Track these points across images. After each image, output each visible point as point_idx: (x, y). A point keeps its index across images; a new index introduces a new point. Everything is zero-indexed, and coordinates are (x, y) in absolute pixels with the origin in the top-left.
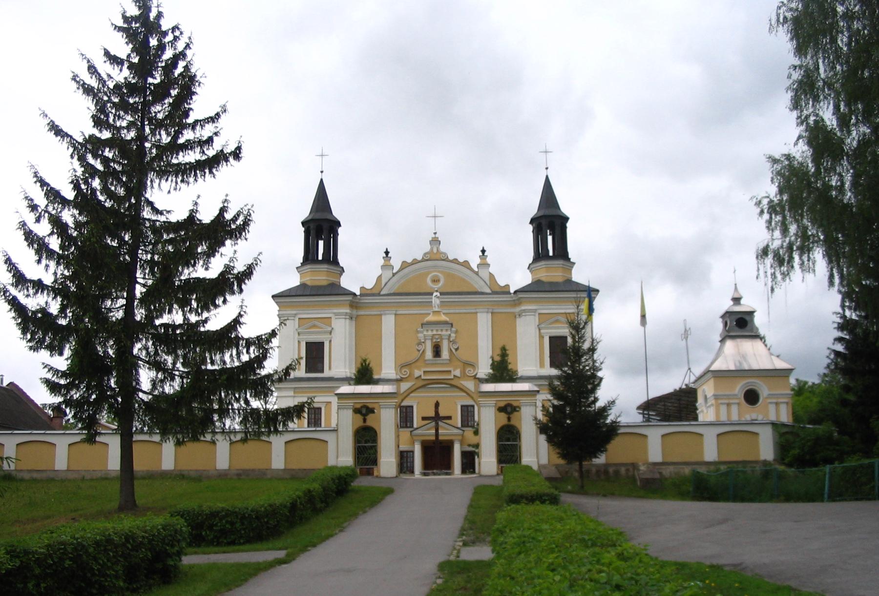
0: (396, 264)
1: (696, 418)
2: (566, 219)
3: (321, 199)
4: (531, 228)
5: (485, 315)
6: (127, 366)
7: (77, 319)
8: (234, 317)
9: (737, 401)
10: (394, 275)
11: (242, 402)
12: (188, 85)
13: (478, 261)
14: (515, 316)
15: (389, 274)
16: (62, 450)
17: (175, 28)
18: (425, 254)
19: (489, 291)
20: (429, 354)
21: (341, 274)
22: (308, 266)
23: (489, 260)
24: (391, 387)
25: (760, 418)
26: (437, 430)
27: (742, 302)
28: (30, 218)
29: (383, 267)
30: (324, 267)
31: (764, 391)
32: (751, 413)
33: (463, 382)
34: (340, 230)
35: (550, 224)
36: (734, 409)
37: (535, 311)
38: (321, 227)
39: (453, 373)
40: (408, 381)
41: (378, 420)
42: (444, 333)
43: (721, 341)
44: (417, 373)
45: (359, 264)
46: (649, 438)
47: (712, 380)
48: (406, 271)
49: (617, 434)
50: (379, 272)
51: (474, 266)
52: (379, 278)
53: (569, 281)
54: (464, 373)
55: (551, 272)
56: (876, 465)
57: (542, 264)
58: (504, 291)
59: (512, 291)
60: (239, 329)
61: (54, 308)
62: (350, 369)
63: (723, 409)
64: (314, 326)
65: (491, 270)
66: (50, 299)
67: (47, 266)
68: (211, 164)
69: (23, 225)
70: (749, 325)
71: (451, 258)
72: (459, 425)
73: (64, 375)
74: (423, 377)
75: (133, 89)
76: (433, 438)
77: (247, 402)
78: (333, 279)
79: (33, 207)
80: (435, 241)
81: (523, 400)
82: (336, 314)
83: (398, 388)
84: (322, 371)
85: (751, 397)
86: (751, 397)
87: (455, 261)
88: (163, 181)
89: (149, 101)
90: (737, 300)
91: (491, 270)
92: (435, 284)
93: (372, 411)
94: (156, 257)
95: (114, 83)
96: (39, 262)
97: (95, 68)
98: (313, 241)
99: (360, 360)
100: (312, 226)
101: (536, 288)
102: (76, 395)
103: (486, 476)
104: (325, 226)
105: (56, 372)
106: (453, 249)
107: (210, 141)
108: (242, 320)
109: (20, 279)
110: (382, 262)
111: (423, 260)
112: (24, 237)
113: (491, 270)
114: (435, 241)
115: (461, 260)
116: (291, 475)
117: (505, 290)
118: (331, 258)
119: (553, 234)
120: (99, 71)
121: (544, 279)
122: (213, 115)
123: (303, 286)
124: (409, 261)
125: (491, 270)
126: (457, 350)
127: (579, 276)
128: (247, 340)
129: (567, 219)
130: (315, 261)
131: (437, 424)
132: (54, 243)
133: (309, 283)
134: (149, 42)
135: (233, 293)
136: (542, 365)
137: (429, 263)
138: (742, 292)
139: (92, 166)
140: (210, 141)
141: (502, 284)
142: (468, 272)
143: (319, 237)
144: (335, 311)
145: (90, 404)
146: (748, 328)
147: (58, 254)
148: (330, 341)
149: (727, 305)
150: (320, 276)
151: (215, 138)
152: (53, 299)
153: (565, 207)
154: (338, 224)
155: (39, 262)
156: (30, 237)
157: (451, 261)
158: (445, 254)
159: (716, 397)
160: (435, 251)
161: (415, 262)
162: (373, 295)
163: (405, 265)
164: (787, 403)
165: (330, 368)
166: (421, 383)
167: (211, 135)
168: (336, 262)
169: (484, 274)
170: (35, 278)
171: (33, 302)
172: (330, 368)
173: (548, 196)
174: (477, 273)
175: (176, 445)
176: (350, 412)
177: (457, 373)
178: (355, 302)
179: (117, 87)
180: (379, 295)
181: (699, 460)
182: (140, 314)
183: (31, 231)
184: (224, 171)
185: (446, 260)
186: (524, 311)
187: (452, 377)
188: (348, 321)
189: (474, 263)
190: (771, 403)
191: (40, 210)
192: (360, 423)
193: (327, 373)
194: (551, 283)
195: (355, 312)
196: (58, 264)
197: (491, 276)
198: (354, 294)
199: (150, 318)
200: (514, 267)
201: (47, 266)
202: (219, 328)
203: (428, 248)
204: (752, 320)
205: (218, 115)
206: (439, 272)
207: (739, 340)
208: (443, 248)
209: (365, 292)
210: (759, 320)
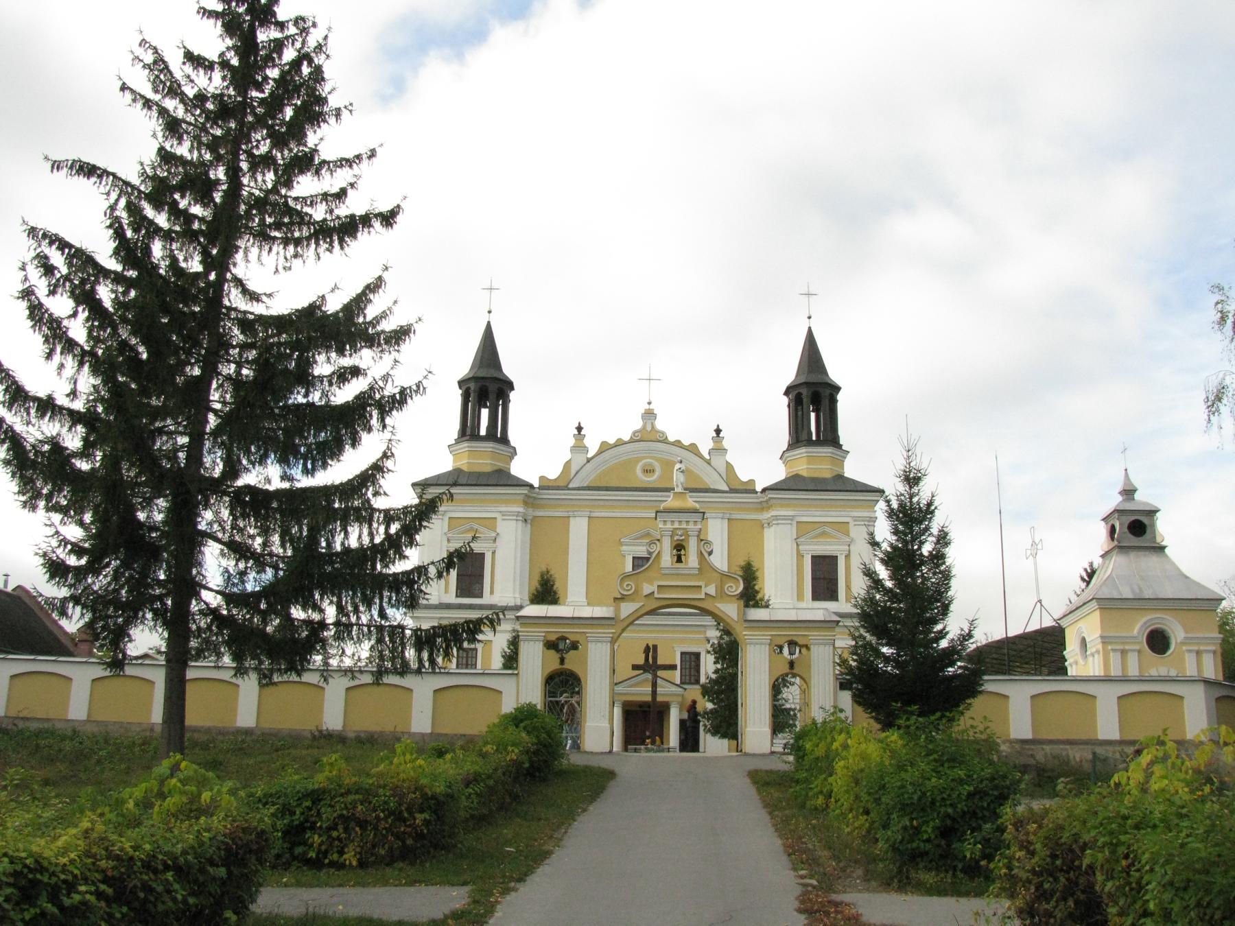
0: (593, 447)
1: (1063, 671)
2: (837, 389)
3: (488, 351)
4: (785, 400)
6: (187, 540)
7: (112, 463)
8: (373, 460)
9: (1137, 647)
10: (589, 460)
11: (375, 613)
12: (313, 111)
13: (711, 445)
15: (580, 459)
16: (77, 692)
17: (299, 20)
18: (634, 433)
19: (727, 489)
20: (667, 559)
21: (511, 458)
22: (466, 444)
23: (725, 444)
24: (605, 609)
25: (1173, 673)
26: (654, 685)
27: (1137, 496)
28: (41, 286)
30: (489, 446)
31: (1177, 634)
32: (1159, 667)
33: (719, 605)
34: (512, 395)
35: (813, 397)
36: (1133, 660)
37: (792, 518)
38: (487, 388)
39: (704, 590)
40: (633, 601)
41: (584, 662)
42: (691, 526)
43: (1102, 556)
44: (647, 589)
46: (1011, 700)
47: (1097, 613)
48: (606, 455)
49: (981, 692)
50: (568, 456)
51: (705, 453)
52: (567, 465)
53: (840, 477)
54: (722, 588)
57: (802, 451)
58: (748, 489)
59: (759, 488)
60: (382, 482)
61: (73, 440)
62: (521, 593)
63: (1115, 659)
65: (729, 457)
66: (66, 429)
67: (61, 366)
68: (350, 228)
69: (27, 293)
70: (1148, 531)
72: (678, 682)
73: (77, 550)
74: (656, 595)
75: (225, 110)
76: (649, 698)
77: (382, 615)
78: (501, 465)
79: (48, 269)
80: (649, 415)
81: (814, 635)
82: (503, 514)
83: (617, 610)
84: (481, 596)
85: (1158, 641)
86: (1158, 641)
87: (678, 444)
88: (265, 253)
89: (252, 120)
91: (729, 458)
93: (574, 646)
94: (245, 372)
95: (196, 89)
96: (49, 356)
97: (164, 62)
98: (473, 411)
99: (537, 577)
100: (472, 386)
101: (792, 484)
102: (99, 583)
103: (754, 755)
104: (492, 388)
105: (64, 542)
106: (672, 426)
107: (341, 195)
108: (389, 464)
109: (18, 395)
110: (572, 442)
111: (631, 441)
112: (27, 312)
113: (729, 458)
114: (649, 415)
115: (686, 443)
116: (437, 747)
117: (748, 488)
118: (497, 435)
119: (817, 411)
120: (172, 68)
121: (805, 474)
122: (350, 155)
123: (457, 472)
124: (612, 441)
125: (729, 457)
126: (710, 553)
127: (853, 470)
128: (387, 512)
129: (838, 389)
130: (475, 436)
131: (655, 677)
132: (78, 331)
133: (465, 468)
134: (255, 37)
135: (370, 430)
136: (800, 597)
139: (151, 222)
140: (341, 195)
141: (744, 478)
143: (481, 403)
144: (503, 509)
145: (118, 605)
146: (1148, 535)
147: (82, 348)
148: (494, 553)
149: (1115, 500)
150: (482, 458)
151: (350, 191)
152: (70, 429)
153: (835, 373)
154: (510, 386)
155: (49, 356)
156: (37, 313)
157: (673, 444)
158: (663, 433)
159: (1105, 640)
160: (649, 428)
161: (620, 443)
162: (558, 488)
163: (605, 447)
164: (1214, 652)
165: (492, 592)
166: (655, 605)
167: (344, 185)
168: (504, 440)
169: (718, 463)
170: (42, 394)
171: (37, 431)
172: (492, 592)
173: (812, 356)
174: (708, 462)
175: (261, 686)
177: (711, 590)
178: (533, 496)
179: (201, 98)
180: (567, 488)
181: (1092, 737)
182: (214, 464)
183: (41, 305)
184: (365, 240)
185: (665, 441)
186: (776, 518)
187: (703, 596)
188: (520, 523)
190: (1190, 651)
191: (58, 276)
192: (554, 665)
193: (487, 599)
194: (814, 480)
195: (531, 512)
196: (81, 364)
197: (729, 467)
198: (531, 486)
199: (232, 470)
200: (762, 456)
201: (61, 366)
202: (345, 480)
203: (638, 425)
204: (1153, 525)
205: (359, 157)
206: (656, 459)
207: (1133, 554)
208: (659, 425)
209: (546, 484)
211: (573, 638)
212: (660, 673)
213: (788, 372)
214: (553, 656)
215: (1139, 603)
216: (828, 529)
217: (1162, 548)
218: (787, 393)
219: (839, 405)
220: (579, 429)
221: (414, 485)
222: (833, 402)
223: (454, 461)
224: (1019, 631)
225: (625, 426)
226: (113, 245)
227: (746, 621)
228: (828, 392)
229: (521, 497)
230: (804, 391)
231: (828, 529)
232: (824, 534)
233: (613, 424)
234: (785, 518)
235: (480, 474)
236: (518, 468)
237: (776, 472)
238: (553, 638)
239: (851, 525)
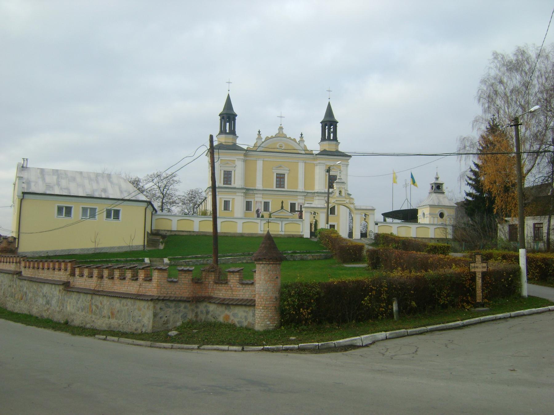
0: (264, 137)
3: (229, 104)
5: (302, 163)
10: (263, 142)
14: (315, 165)
35: (329, 123)
37: (324, 163)
45: (245, 137)
48: (266, 142)
53: (337, 151)
55: (328, 146)
56: (270, 203)
64: (227, 163)
65: (305, 143)
71: (288, 137)
80: (281, 128)
82: (238, 159)
84: (231, 184)
85: (442, 215)
86: (442, 215)
87: (290, 138)
90: (437, 179)
92: (279, 148)
101: (324, 153)
110: (257, 136)
114: (281, 128)
115: (292, 138)
118: (233, 132)
121: (327, 149)
125: (305, 143)
127: (341, 149)
137: (279, 138)
138: (439, 176)
142: (295, 143)
149: (434, 181)
159: (430, 214)
161: (272, 137)
163: (267, 139)
176: (309, 214)
180: (256, 151)
189: (298, 140)
193: (233, 185)
200: (313, 141)
204: (442, 187)
208: (285, 131)
210: (444, 187)
215: (438, 206)
217: (444, 193)
220: (259, 132)
221: (383, 214)
225: (273, 132)
233: (270, 132)
234: (322, 163)
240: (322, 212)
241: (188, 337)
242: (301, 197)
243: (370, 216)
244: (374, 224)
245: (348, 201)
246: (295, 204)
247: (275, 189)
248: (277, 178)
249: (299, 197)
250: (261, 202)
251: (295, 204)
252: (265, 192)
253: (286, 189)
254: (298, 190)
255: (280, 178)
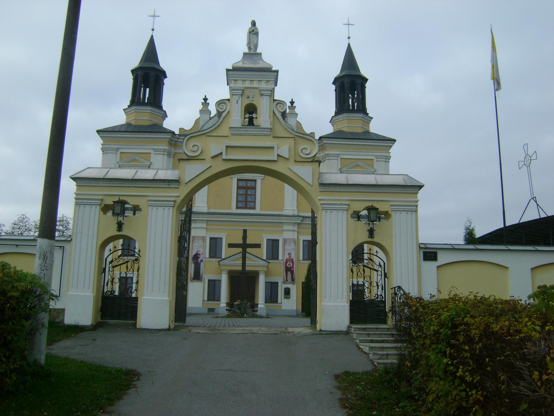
4: (334, 87)
15: (206, 117)
26: (244, 259)
29: (201, 111)
39: (276, 152)
52: (197, 121)
53: (368, 132)
64: (134, 160)
72: (265, 258)
74: (224, 157)
76: (240, 268)
101: (338, 135)
110: (201, 107)
121: (345, 130)
127: (374, 128)
129: (366, 80)
133: (133, 123)
176: (96, 211)
178: (175, 139)
187: (275, 158)
188: (166, 156)
194: (351, 133)
211: (132, 202)
212: (248, 250)
213: (335, 69)
214: (110, 219)
216: (360, 163)
218: (334, 83)
219: (367, 89)
222: (363, 88)
223: (127, 119)
224: (515, 221)
226: (304, 280)
227: (322, 185)
228: (359, 81)
229: (167, 140)
230: (346, 81)
231: (360, 163)
232: (357, 166)
235: (142, 126)
236: (167, 124)
237: (329, 129)
238: (109, 201)
239: (375, 160)
240: (157, 203)
241: (479, 307)
242: (291, 227)
243: (396, 217)
244: (415, 255)
245: (284, 148)
246: (278, 241)
247: (234, 210)
248: (239, 187)
249: (285, 227)
250: (203, 239)
251: (278, 241)
252: (211, 218)
253: (258, 211)
254: (285, 213)
255: (246, 188)
